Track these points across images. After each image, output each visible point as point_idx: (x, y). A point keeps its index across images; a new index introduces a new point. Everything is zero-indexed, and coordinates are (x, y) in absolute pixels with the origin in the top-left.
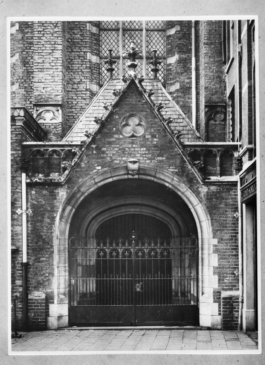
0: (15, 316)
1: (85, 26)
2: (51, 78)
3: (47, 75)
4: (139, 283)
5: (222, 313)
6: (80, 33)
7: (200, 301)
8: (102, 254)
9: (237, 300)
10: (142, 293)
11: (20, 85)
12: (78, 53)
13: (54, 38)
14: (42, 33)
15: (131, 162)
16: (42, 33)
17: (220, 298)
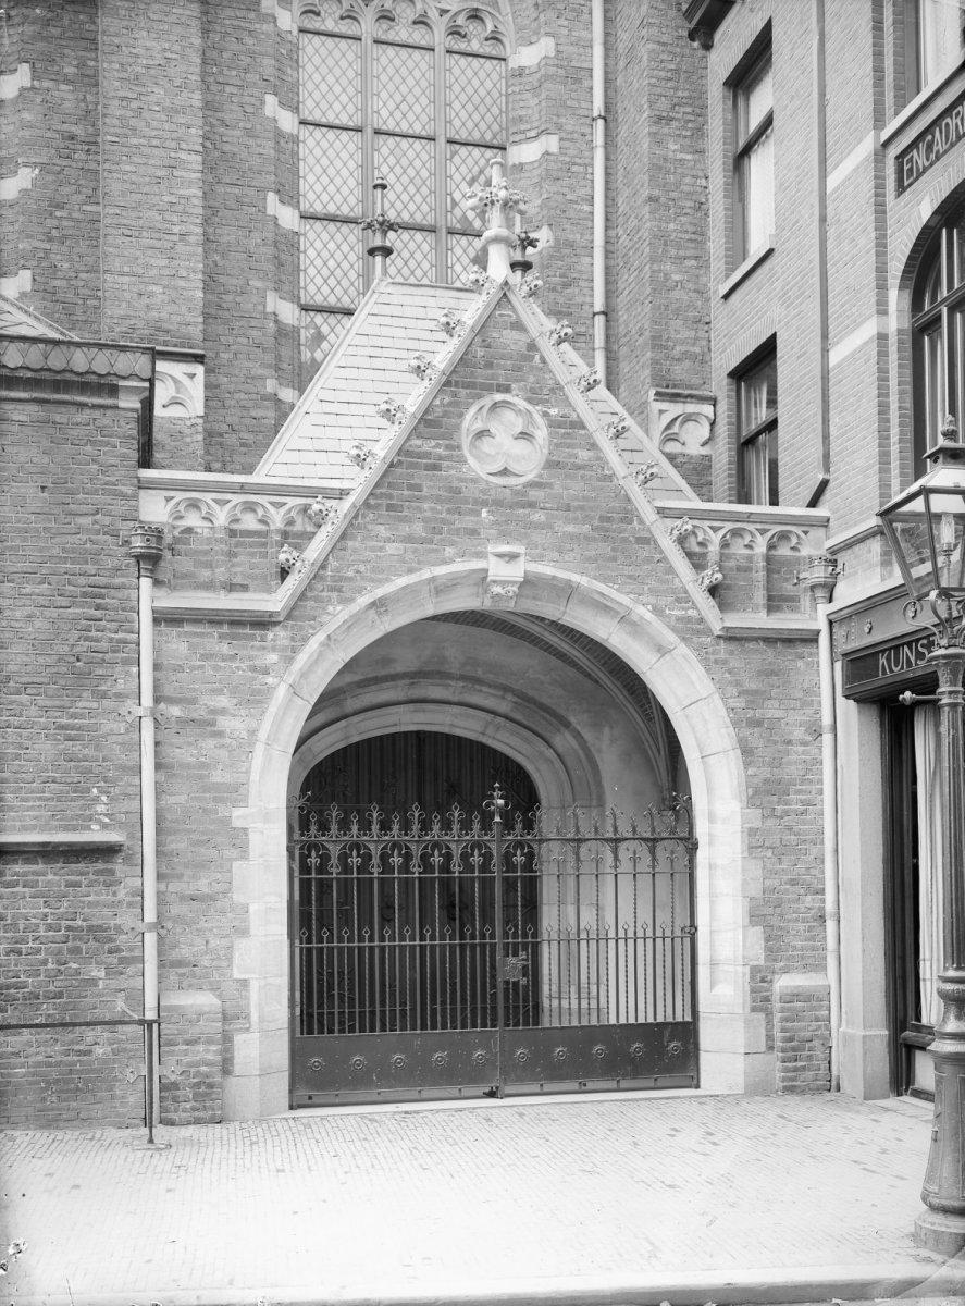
0: (685, 1044)
1: (258, 103)
2: (165, 262)
3: (150, 252)
4: (515, 954)
5: (779, 1044)
6: (241, 125)
7: (287, 1031)
8: (314, 860)
9: (336, 1028)
10: (526, 987)
11: (34, 280)
12: (237, 191)
13: (174, 127)
14: (134, 105)
15: (500, 556)
16: (134, 105)
17: (767, 999)
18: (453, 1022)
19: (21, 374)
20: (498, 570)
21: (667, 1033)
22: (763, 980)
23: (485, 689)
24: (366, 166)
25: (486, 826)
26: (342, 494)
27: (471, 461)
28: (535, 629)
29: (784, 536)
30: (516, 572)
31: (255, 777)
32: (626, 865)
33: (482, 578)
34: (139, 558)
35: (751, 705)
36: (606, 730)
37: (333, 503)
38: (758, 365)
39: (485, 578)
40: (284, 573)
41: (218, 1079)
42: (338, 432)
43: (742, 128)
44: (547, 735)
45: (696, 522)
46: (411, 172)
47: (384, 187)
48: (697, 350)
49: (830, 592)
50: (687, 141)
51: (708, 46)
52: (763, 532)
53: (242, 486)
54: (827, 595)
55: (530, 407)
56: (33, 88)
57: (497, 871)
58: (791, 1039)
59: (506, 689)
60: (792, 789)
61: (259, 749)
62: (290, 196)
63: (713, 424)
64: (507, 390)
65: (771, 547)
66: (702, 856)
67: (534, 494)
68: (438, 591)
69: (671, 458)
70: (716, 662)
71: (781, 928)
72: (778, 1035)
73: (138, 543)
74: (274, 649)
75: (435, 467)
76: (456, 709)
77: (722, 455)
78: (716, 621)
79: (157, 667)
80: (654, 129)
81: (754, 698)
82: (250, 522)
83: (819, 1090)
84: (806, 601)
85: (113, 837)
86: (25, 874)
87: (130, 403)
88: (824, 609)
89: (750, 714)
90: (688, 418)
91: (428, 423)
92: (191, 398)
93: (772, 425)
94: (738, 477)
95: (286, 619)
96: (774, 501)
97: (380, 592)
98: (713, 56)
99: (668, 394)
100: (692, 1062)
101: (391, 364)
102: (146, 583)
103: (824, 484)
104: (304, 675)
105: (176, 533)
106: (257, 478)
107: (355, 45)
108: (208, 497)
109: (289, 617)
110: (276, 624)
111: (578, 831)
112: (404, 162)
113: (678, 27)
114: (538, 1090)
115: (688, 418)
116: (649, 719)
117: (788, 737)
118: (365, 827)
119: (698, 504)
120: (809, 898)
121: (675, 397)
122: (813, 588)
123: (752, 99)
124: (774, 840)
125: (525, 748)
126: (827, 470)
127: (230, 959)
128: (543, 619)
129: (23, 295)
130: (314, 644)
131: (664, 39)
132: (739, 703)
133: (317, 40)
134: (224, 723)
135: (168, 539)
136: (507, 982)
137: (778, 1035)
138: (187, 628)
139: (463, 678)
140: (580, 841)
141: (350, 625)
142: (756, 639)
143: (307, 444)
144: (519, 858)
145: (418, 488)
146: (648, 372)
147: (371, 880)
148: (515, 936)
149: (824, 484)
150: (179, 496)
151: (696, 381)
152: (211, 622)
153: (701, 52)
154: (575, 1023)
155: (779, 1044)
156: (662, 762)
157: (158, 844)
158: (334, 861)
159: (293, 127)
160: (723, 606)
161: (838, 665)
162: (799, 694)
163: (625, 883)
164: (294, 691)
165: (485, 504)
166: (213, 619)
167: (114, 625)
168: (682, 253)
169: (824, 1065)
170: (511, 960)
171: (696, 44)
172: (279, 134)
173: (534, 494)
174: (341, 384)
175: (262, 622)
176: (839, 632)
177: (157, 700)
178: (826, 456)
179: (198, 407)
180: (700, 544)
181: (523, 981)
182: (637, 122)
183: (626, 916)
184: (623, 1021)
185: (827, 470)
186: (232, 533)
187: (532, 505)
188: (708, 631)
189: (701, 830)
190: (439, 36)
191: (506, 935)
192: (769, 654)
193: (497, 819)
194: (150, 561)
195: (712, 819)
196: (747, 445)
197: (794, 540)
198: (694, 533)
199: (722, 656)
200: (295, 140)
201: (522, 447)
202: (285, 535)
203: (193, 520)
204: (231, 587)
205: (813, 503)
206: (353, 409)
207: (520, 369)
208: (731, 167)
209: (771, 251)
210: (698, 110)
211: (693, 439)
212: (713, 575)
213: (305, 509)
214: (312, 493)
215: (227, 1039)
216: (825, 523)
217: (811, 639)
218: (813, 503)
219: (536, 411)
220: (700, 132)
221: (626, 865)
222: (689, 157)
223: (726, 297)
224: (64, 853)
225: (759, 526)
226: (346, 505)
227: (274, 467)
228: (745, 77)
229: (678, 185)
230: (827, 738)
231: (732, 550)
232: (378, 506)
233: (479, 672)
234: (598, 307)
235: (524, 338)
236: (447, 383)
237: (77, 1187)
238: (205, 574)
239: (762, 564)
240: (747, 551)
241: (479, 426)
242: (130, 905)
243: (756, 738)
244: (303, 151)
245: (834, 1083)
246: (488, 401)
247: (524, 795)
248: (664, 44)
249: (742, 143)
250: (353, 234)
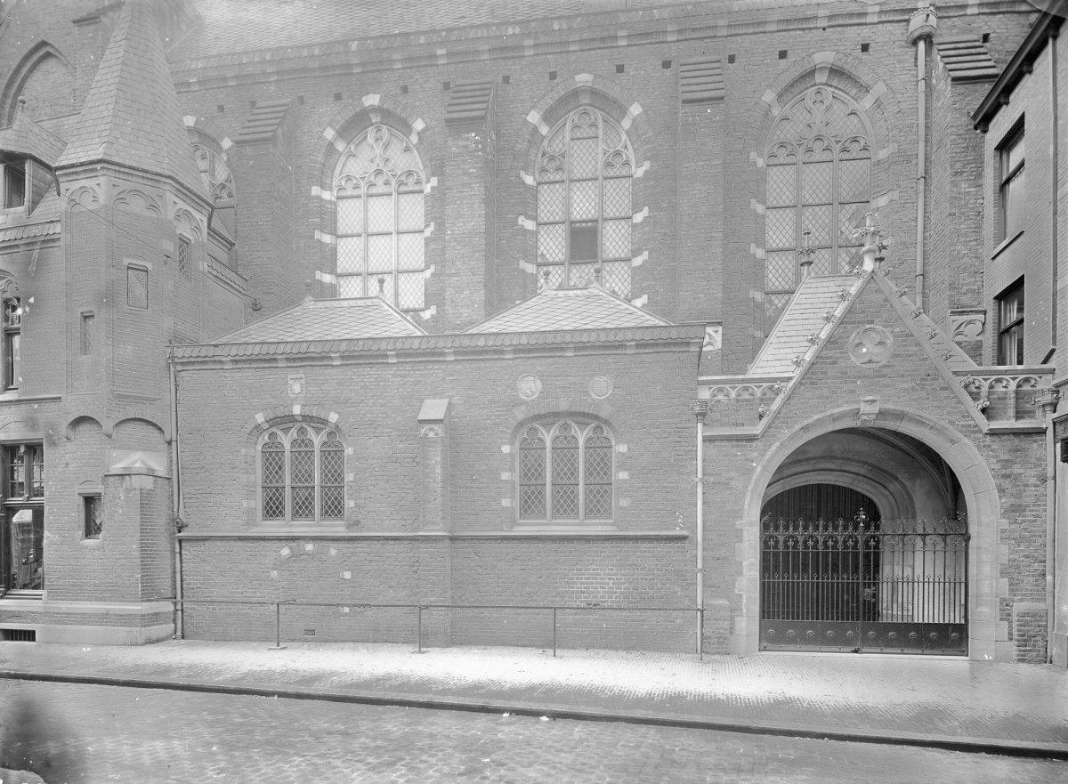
0: (961, 634)
17: (1009, 615)
18: (823, 616)
19: (650, 342)
20: (865, 408)
21: (950, 629)
22: (1007, 605)
23: (853, 463)
24: (798, 224)
25: (856, 528)
26: (790, 379)
27: (853, 358)
28: (881, 434)
29: (1027, 380)
30: (875, 409)
31: (746, 507)
32: (929, 546)
33: (856, 413)
34: (697, 415)
35: (1004, 467)
36: (918, 481)
37: (784, 384)
38: (1014, 291)
39: (858, 413)
40: (761, 417)
41: (728, 635)
42: (787, 351)
43: (1005, 171)
44: (886, 485)
45: (975, 377)
46: (820, 222)
47: (809, 233)
48: (976, 287)
49: (1054, 407)
50: (972, 182)
51: (985, 131)
52: (1014, 379)
53: (743, 380)
54: (1053, 409)
55: (884, 329)
56: (649, 216)
57: (861, 549)
58: (1023, 636)
59: (865, 463)
60: (1028, 509)
61: (749, 494)
62: (761, 243)
63: (984, 324)
64: (872, 322)
65: (1019, 386)
66: (971, 543)
67: (885, 371)
68: (834, 420)
69: (959, 344)
70: (984, 446)
71: (1018, 580)
72: (1015, 632)
73: (697, 409)
74: (756, 451)
75: (834, 363)
76: (838, 473)
77: (989, 340)
78: (985, 425)
79: (704, 460)
80: (953, 179)
81: (1007, 463)
82: (746, 396)
83: (1040, 662)
84: (1039, 413)
85: (685, 533)
86: (649, 548)
87: (695, 349)
88: (1051, 416)
89: (1004, 472)
90: (970, 322)
91: (831, 341)
92: (716, 341)
93: (1020, 322)
94: (998, 348)
95: (762, 437)
96: (1020, 362)
97: (806, 422)
98: (988, 136)
99: (958, 312)
100: (965, 643)
101: (812, 316)
102: (700, 425)
103: (1053, 351)
104: (769, 461)
105: (713, 403)
106: (749, 376)
107: (793, 167)
108: (727, 386)
109: (763, 436)
110: (757, 439)
111: (904, 531)
112: (817, 217)
113: (967, 125)
114: (879, 651)
115: (970, 322)
116: (942, 474)
117: (1026, 483)
118: (835, 528)
119: (975, 367)
120: (1036, 564)
121: (962, 313)
122: (1044, 406)
123: (1011, 154)
124: (1016, 535)
125: (873, 490)
126: (1054, 343)
127: (734, 585)
128: (885, 429)
129: (644, 305)
130: (774, 448)
131: (960, 132)
132: (997, 467)
133: (775, 169)
134: (734, 484)
135: (710, 405)
136: (865, 600)
137: (1015, 632)
138: (717, 443)
139: (843, 458)
140: (925, 535)
141: (792, 438)
142: (1009, 434)
143: (771, 358)
144: (872, 543)
145: (826, 373)
146: (946, 302)
147: (818, 552)
148: (869, 579)
149: (1053, 351)
150: (715, 387)
151: (974, 303)
152: (728, 440)
153: (982, 135)
154: (900, 621)
155: (1015, 637)
156: (949, 496)
157: (703, 535)
158: (781, 543)
159: (580, 82)
160: (989, 418)
161: (1058, 445)
162: (1033, 460)
163: (929, 556)
164: (764, 468)
165: (859, 377)
166: (729, 438)
167: (686, 444)
168: (968, 239)
169: (1043, 650)
170: (867, 590)
171: (978, 131)
172: (757, 215)
173: (885, 371)
174: (787, 328)
175: (751, 439)
176: (1060, 428)
177: (704, 475)
178: (1054, 337)
179: (719, 345)
180: (977, 388)
181: (873, 600)
182: (942, 175)
183: (929, 571)
184: (926, 621)
185: (1054, 343)
186: (738, 401)
187: (884, 376)
188: (981, 431)
189: (973, 530)
190: (836, 154)
191: (865, 579)
192: (1016, 441)
193: (861, 524)
194: (702, 415)
195: (980, 524)
196: (1003, 333)
197: (1033, 382)
198: (974, 383)
199: (987, 443)
200: (764, 217)
201: (878, 350)
202: (762, 400)
203: (720, 397)
204: (737, 425)
205: (1045, 362)
206: (793, 339)
207: (879, 312)
208: (998, 191)
209: (1022, 233)
210: (979, 165)
211: (971, 332)
212: (983, 403)
213: (771, 387)
214: (775, 380)
215: (732, 618)
216: (1052, 371)
217: (1042, 432)
218: (1045, 362)
219: (887, 331)
220: (979, 176)
221: (929, 546)
222: (973, 189)
223: (994, 258)
224: (665, 539)
225: (1012, 376)
226: (791, 384)
227: (758, 370)
228: (1006, 145)
229: (966, 205)
230: (1050, 483)
231: (995, 389)
232: (806, 383)
233: (850, 455)
234: (919, 272)
235: (883, 297)
236: (842, 323)
237: (674, 674)
238: (726, 420)
239: (1013, 395)
240: (1004, 389)
241: (857, 341)
242: (691, 561)
243: (1006, 484)
244: (767, 221)
245: (1048, 659)
246: (862, 328)
247: (874, 516)
248: (960, 135)
249: (1004, 178)
250: (791, 255)
